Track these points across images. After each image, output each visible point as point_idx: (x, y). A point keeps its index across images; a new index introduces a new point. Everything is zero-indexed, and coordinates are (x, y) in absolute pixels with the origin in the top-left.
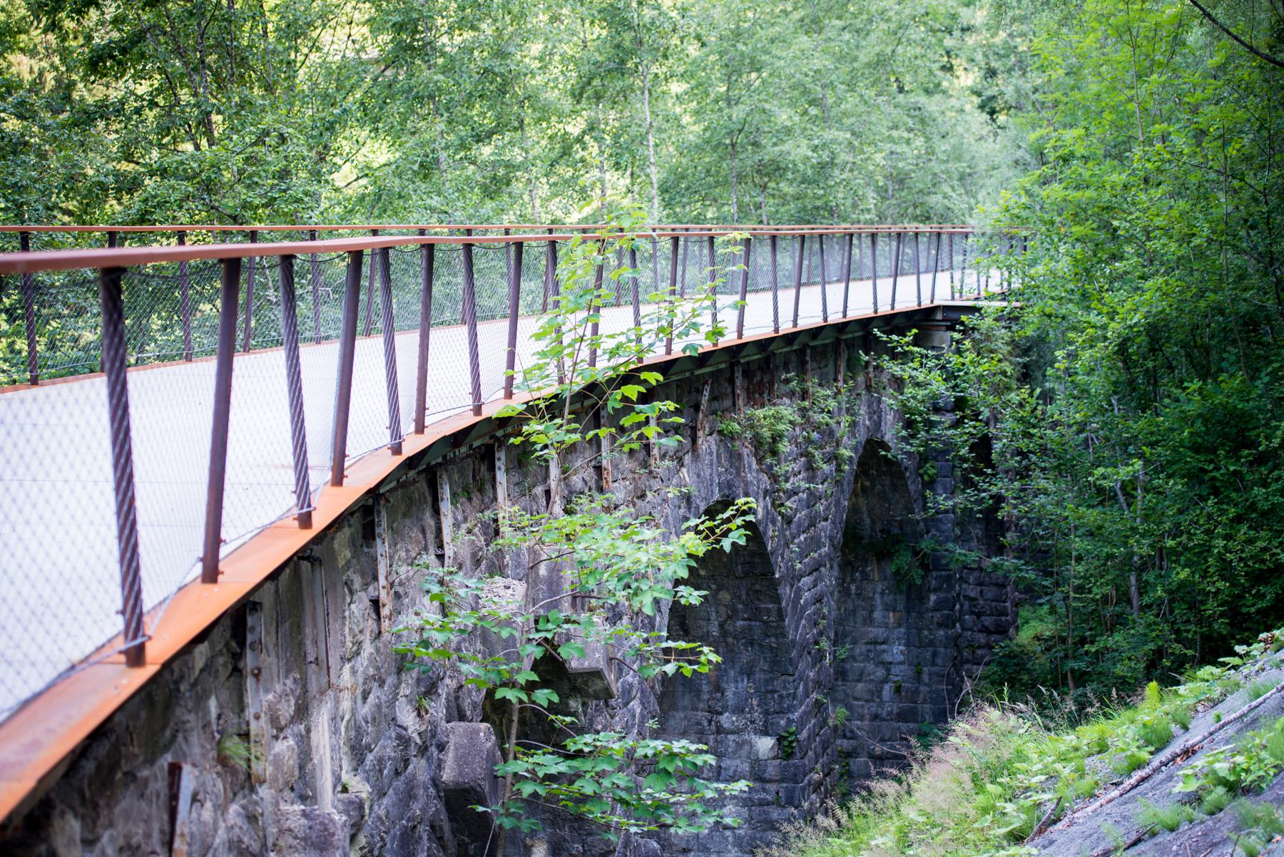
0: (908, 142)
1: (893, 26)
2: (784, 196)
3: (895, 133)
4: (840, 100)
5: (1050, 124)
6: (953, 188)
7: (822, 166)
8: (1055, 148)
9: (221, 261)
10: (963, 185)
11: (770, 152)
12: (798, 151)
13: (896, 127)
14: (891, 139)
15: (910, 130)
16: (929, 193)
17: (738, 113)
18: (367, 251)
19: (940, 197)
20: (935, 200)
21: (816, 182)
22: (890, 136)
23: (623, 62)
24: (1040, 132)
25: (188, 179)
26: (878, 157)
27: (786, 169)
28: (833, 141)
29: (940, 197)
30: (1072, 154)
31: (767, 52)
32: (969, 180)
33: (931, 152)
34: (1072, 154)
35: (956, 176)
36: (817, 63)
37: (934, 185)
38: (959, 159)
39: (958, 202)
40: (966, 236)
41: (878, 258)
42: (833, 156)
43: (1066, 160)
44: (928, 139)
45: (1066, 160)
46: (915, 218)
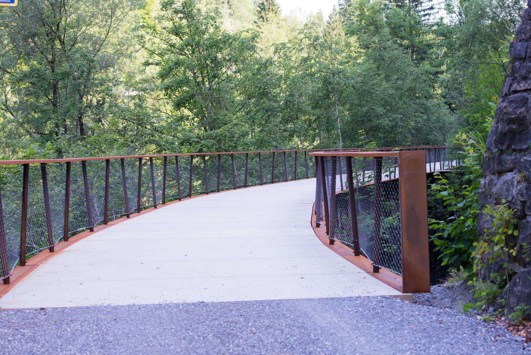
0: (421, 117)
1: (415, 77)
2: (380, 137)
3: (416, 114)
4: (397, 103)
5: (470, 112)
6: (437, 132)
7: (393, 127)
8: (472, 120)
9: (375, 158)
10: (441, 131)
11: (376, 122)
12: (385, 122)
13: (416, 112)
14: (415, 116)
15: (422, 113)
16: (428, 135)
17: (365, 109)
18: (384, 158)
19: (433, 136)
20: (431, 137)
21: (391, 132)
22: (415, 115)
23: (329, 95)
24: (467, 115)
25: (214, 139)
26: (412, 123)
27: (381, 128)
28: (397, 118)
29: (433, 136)
30: (477, 122)
31: (373, 89)
32: (442, 130)
33: (429, 120)
34: (477, 122)
35: (438, 128)
36: (390, 92)
37: (430, 132)
38: (439, 122)
39: (440, 137)
40: (445, 149)
41: (50, 184)
42: (397, 123)
43: (476, 124)
44: (428, 116)
45: (476, 124)
46: (424, 143)
